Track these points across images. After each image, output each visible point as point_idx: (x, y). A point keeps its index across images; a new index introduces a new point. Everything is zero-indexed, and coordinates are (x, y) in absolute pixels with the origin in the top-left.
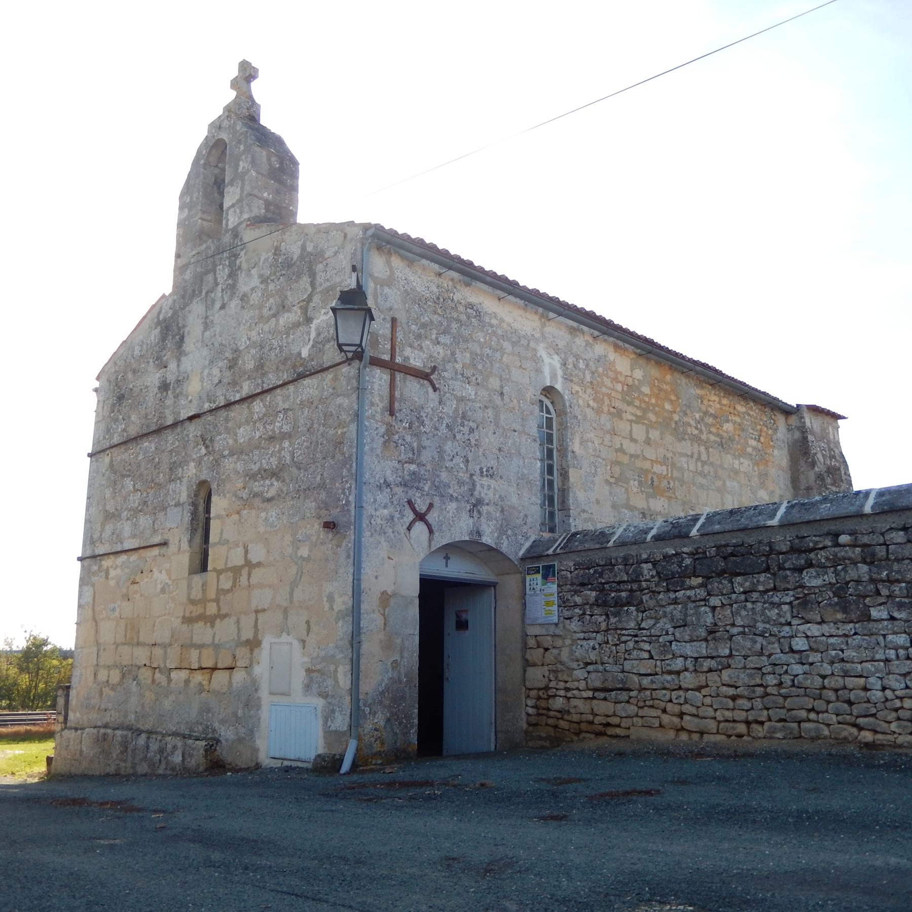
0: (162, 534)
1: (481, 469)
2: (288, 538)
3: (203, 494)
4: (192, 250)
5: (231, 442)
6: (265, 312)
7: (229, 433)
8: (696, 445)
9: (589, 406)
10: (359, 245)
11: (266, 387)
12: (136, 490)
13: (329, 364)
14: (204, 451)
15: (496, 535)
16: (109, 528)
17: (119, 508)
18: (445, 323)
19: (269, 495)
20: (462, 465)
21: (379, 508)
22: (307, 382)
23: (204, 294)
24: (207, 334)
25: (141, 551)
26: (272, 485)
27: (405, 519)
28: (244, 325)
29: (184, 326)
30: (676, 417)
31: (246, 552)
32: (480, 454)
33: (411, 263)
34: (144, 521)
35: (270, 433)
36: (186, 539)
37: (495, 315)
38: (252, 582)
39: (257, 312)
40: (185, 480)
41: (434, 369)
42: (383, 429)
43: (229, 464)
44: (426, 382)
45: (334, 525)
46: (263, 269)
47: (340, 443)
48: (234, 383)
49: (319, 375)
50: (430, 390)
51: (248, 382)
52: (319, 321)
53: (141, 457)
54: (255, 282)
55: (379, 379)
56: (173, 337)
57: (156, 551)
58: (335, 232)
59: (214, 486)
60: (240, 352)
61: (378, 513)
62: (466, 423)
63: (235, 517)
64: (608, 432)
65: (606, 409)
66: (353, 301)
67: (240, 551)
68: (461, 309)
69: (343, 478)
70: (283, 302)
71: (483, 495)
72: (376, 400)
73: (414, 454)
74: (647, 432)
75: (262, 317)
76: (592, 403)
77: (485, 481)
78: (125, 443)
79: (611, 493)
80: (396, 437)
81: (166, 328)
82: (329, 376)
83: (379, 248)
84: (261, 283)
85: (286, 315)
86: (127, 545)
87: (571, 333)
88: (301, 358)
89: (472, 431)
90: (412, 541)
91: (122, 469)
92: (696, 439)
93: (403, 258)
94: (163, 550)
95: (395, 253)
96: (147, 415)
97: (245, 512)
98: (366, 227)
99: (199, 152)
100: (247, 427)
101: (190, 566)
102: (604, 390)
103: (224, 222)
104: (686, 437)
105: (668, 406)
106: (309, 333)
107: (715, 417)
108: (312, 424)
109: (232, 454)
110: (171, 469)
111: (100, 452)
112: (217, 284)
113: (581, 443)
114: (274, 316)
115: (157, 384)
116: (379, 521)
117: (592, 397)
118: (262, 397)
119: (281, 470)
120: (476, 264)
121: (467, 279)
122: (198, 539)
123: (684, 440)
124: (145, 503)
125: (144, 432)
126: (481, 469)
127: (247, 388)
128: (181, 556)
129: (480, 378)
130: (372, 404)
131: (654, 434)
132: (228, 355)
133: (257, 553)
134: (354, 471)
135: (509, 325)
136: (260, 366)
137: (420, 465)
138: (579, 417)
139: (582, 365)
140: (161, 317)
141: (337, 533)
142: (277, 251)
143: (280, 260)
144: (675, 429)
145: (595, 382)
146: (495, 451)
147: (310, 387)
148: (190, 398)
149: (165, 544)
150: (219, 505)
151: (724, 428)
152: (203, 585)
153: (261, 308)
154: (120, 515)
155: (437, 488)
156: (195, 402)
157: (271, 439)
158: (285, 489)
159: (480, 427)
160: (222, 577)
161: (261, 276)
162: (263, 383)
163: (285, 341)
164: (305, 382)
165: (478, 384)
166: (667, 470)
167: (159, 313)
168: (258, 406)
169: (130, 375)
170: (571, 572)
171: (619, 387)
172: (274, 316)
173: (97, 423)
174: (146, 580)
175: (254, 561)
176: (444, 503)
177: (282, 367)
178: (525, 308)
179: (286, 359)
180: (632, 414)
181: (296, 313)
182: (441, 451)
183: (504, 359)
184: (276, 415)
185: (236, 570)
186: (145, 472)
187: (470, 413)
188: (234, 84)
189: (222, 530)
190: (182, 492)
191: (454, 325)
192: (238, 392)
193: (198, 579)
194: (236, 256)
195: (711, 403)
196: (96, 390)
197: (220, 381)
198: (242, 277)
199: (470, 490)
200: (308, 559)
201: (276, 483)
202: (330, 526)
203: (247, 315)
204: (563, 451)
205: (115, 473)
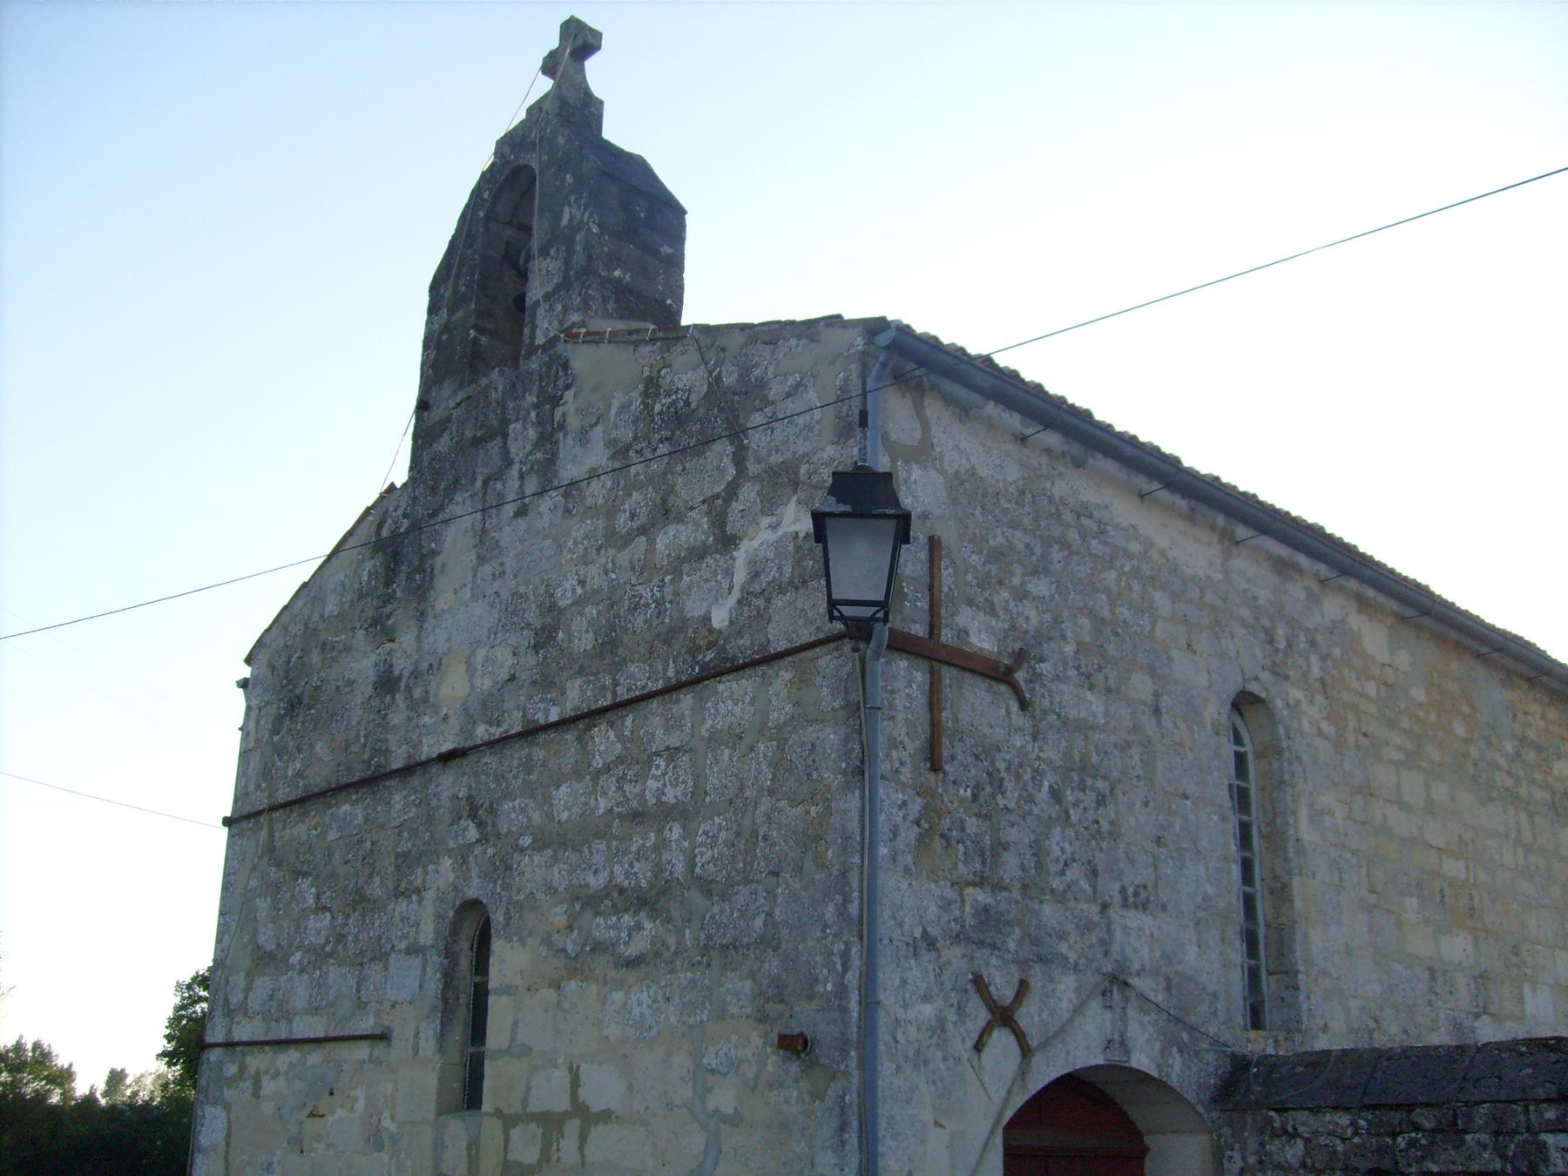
0: (377, 1013)
1: (1123, 891)
2: (682, 1061)
3: (469, 929)
4: (455, 393)
5: (537, 817)
6: (622, 522)
7: (532, 796)
8: (1511, 812)
9: (1320, 733)
10: (854, 368)
11: (623, 694)
12: (322, 909)
13: (783, 645)
14: (473, 833)
15: (1157, 1045)
16: (263, 984)
17: (284, 943)
18: (1038, 550)
19: (633, 950)
20: (1084, 885)
21: (914, 1000)
22: (723, 686)
23: (479, 483)
24: (487, 569)
25: (331, 1046)
26: (639, 927)
27: (969, 1025)
28: (571, 551)
29: (434, 553)
30: (1474, 752)
31: (575, 1082)
32: (1121, 854)
33: (964, 412)
34: (338, 978)
35: (634, 803)
36: (431, 1032)
37: (1133, 532)
38: (589, 1159)
39: (601, 523)
40: (430, 895)
41: (1020, 656)
42: (916, 806)
43: (533, 869)
44: (1003, 688)
45: (806, 1042)
46: (616, 426)
47: (817, 839)
48: (546, 683)
49: (760, 670)
50: (1014, 706)
51: (579, 681)
52: (755, 544)
53: (332, 835)
54: (598, 455)
55: (903, 682)
56: (410, 577)
57: (362, 1051)
58: (793, 341)
59: (498, 918)
60: (561, 611)
61: (911, 1015)
62: (1089, 782)
63: (548, 994)
64: (1358, 790)
65: (1351, 738)
66: (863, 497)
67: (561, 1076)
68: (1068, 517)
69: (825, 926)
70: (664, 501)
71: (1128, 952)
72: (900, 732)
73: (984, 863)
74: (1428, 786)
75: (614, 533)
76: (1325, 726)
77: (1134, 918)
78: (301, 801)
79: (1371, 929)
80: (946, 823)
81: (390, 551)
82: (784, 675)
83: (900, 379)
84: (613, 457)
85: (672, 530)
86: (305, 1027)
87: (1278, 572)
88: (711, 630)
89: (1101, 801)
90: (986, 1079)
91: (292, 858)
92: (1512, 798)
93: (948, 400)
94: (380, 1050)
95: (933, 387)
96: (348, 745)
97: (573, 984)
98: (875, 327)
99: (476, 193)
100: (576, 786)
101: (440, 1094)
102: (1346, 696)
103: (526, 331)
104: (1495, 794)
105: (1459, 729)
106: (729, 573)
107: (1539, 748)
108: (742, 788)
109: (540, 844)
110: (398, 868)
111: (248, 817)
112: (509, 463)
113: (1311, 819)
114: (643, 530)
115: (372, 676)
116: (913, 1032)
117: (1325, 713)
118: (611, 716)
119: (663, 893)
120: (1098, 416)
121: (1077, 450)
122: (457, 1034)
123: (1491, 799)
124: (341, 938)
125: (344, 780)
126: (1123, 891)
127: (576, 695)
128: (417, 1072)
129: (1113, 675)
130: (894, 744)
131: (1440, 791)
132: (533, 617)
133: (603, 1088)
134: (854, 909)
135: (1162, 552)
136: (609, 646)
137: (998, 887)
138: (1305, 758)
139: (1302, 642)
140: (385, 533)
141: (812, 1064)
142: (652, 387)
143: (658, 408)
144: (1474, 779)
145: (1329, 680)
146: (1148, 845)
147: (732, 701)
148: (445, 711)
149: (382, 1037)
150: (509, 961)
151: (1556, 771)
152: (469, 1147)
153: (610, 511)
154: (286, 957)
155: (1036, 942)
156: (455, 724)
157: (638, 816)
158: (672, 941)
159: (1118, 792)
160: (515, 1133)
161: (610, 443)
162: (616, 684)
163: (668, 589)
164: (721, 687)
165: (1109, 690)
166: (1467, 868)
167: (380, 526)
168: (604, 741)
169: (315, 657)
170: (1343, 1140)
171: (1371, 689)
172: (643, 530)
173: (244, 755)
174: (340, 1113)
175: (596, 1106)
176: (1051, 979)
177: (662, 649)
178: (1191, 518)
179: (674, 630)
180: (1399, 748)
181: (697, 525)
182: (1038, 850)
183: (1158, 633)
184: (649, 763)
185: (551, 1123)
186: (342, 870)
187: (1095, 759)
188: (550, 66)
189: (516, 1022)
190: (425, 921)
191: (1056, 554)
192: (554, 702)
193: (457, 1130)
194: (556, 401)
195: (1529, 718)
196: (244, 684)
197: (513, 678)
198: (567, 446)
199: (1103, 943)
200: (735, 1120)
201: (648, 925)
202: (794, 1045)
203: (579, 529)
204: (1277, 839)
205: (279, 865)
